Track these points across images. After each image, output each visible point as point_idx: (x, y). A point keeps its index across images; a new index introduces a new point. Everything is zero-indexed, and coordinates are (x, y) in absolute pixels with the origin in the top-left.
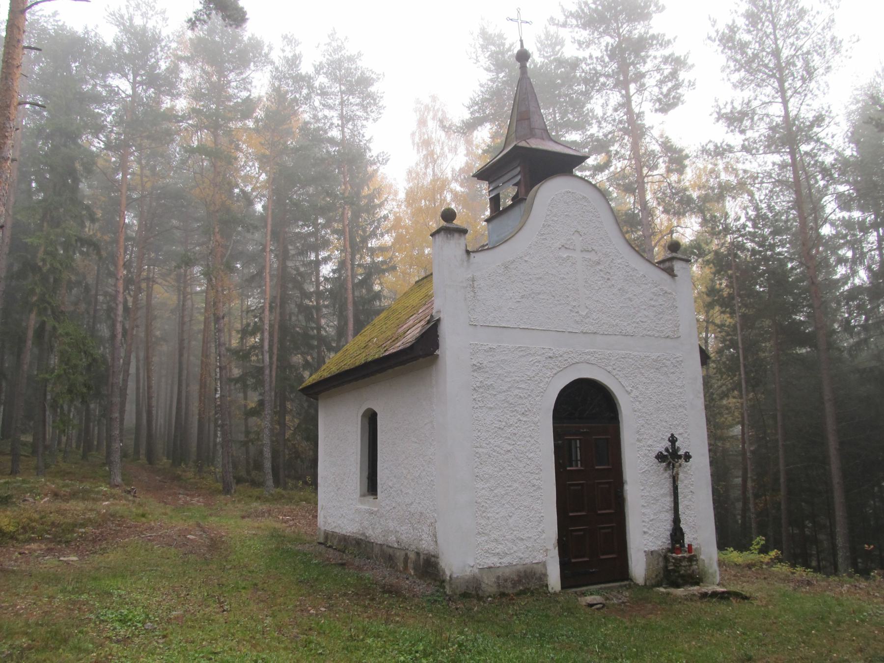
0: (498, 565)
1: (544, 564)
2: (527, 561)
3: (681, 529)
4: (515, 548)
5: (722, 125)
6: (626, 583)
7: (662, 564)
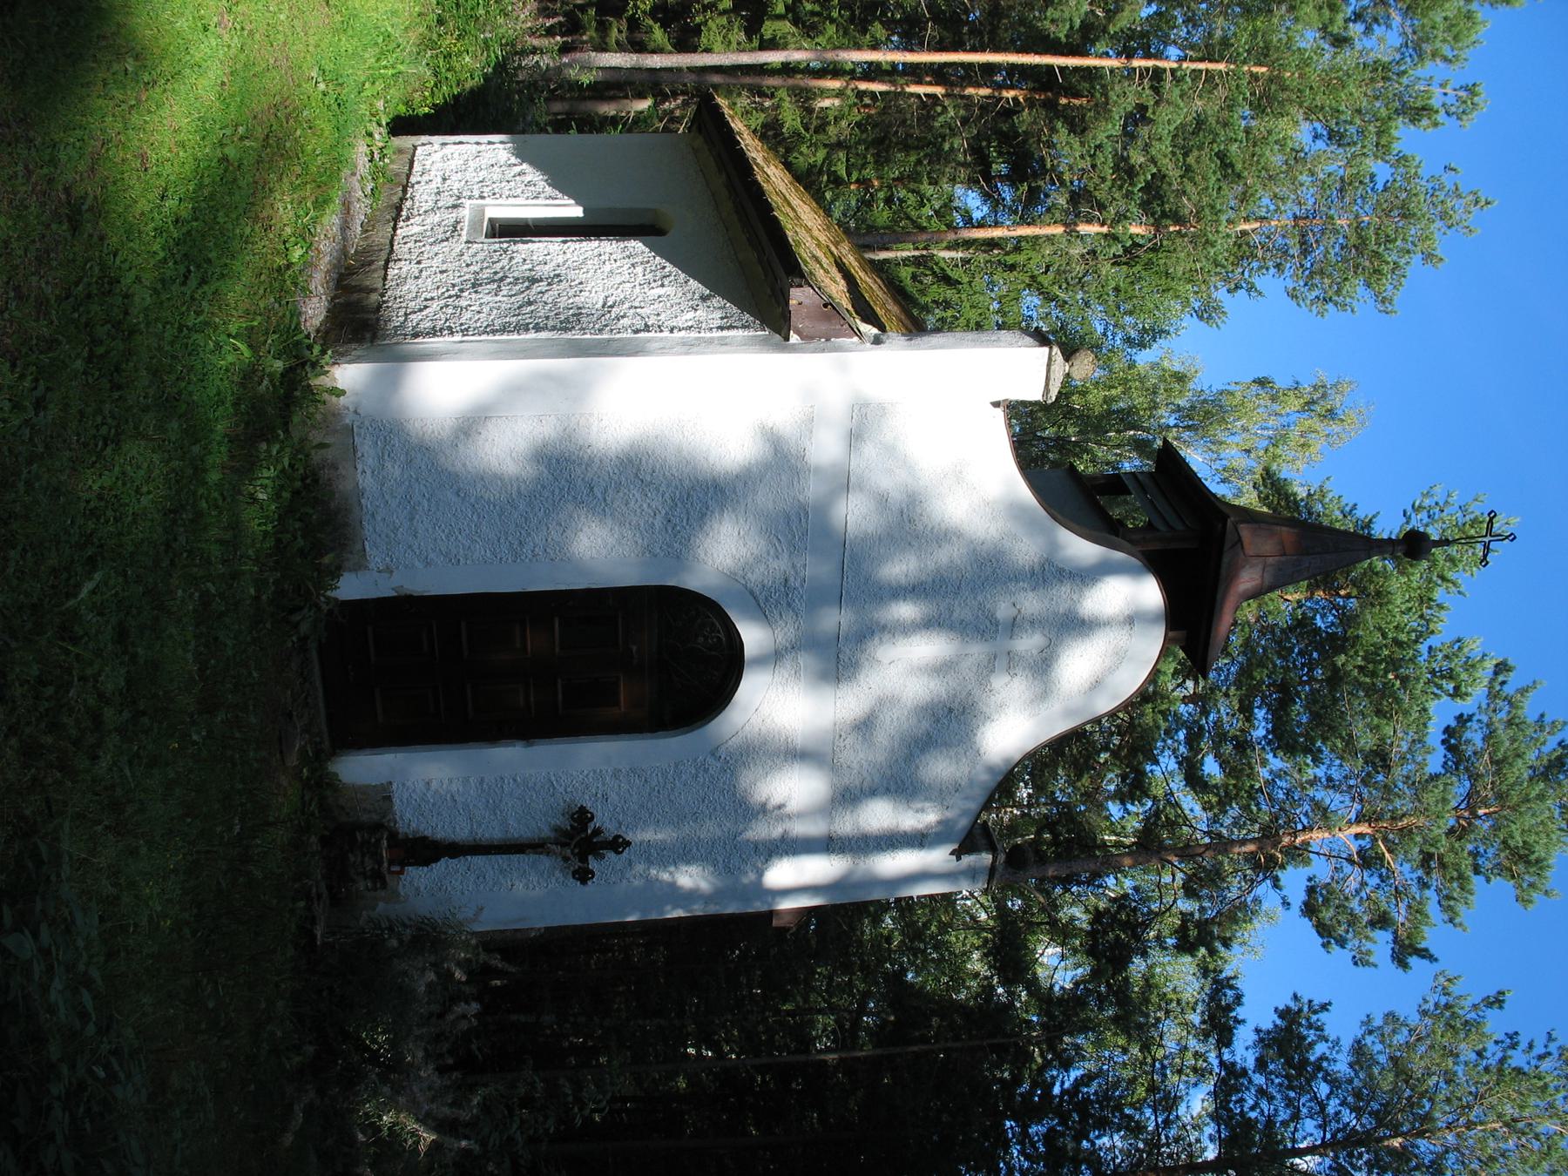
0: (360, 467)
1: (361, 566)
2: (368, 529)
3: (437, 860)
4: (393, 503)
5: (1268, 1021)
6: (326, 745)
7: (365, 818)
